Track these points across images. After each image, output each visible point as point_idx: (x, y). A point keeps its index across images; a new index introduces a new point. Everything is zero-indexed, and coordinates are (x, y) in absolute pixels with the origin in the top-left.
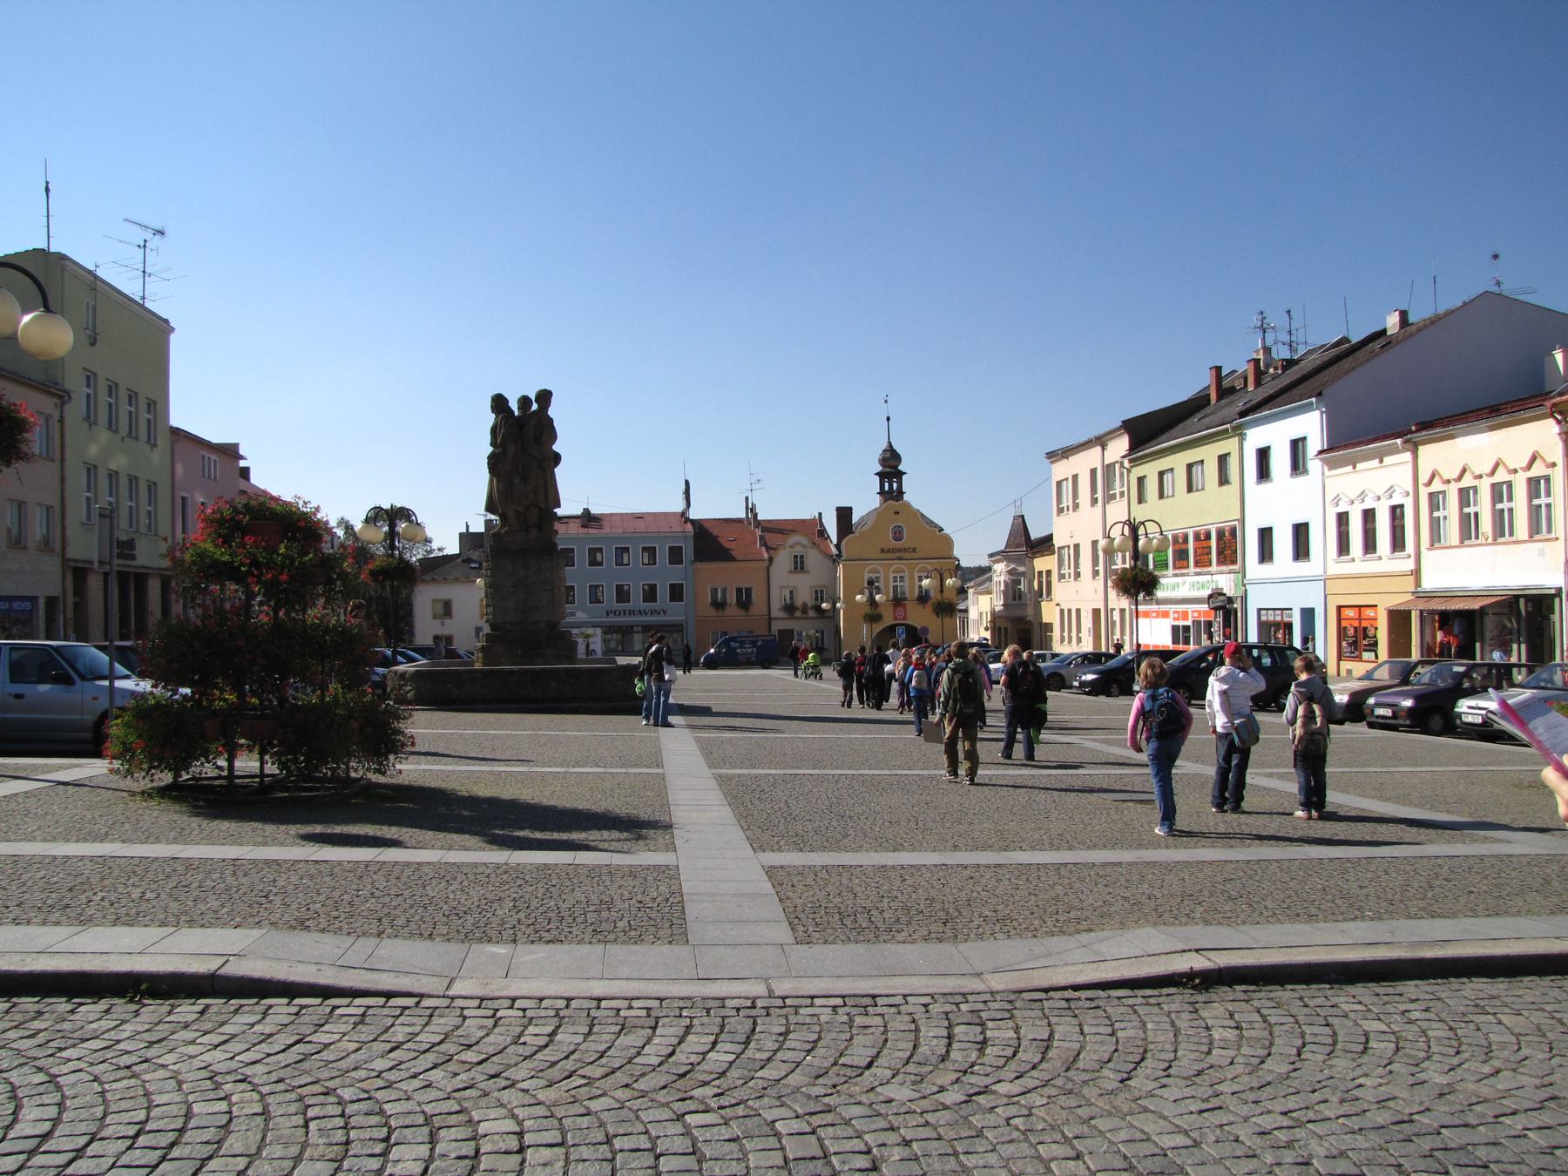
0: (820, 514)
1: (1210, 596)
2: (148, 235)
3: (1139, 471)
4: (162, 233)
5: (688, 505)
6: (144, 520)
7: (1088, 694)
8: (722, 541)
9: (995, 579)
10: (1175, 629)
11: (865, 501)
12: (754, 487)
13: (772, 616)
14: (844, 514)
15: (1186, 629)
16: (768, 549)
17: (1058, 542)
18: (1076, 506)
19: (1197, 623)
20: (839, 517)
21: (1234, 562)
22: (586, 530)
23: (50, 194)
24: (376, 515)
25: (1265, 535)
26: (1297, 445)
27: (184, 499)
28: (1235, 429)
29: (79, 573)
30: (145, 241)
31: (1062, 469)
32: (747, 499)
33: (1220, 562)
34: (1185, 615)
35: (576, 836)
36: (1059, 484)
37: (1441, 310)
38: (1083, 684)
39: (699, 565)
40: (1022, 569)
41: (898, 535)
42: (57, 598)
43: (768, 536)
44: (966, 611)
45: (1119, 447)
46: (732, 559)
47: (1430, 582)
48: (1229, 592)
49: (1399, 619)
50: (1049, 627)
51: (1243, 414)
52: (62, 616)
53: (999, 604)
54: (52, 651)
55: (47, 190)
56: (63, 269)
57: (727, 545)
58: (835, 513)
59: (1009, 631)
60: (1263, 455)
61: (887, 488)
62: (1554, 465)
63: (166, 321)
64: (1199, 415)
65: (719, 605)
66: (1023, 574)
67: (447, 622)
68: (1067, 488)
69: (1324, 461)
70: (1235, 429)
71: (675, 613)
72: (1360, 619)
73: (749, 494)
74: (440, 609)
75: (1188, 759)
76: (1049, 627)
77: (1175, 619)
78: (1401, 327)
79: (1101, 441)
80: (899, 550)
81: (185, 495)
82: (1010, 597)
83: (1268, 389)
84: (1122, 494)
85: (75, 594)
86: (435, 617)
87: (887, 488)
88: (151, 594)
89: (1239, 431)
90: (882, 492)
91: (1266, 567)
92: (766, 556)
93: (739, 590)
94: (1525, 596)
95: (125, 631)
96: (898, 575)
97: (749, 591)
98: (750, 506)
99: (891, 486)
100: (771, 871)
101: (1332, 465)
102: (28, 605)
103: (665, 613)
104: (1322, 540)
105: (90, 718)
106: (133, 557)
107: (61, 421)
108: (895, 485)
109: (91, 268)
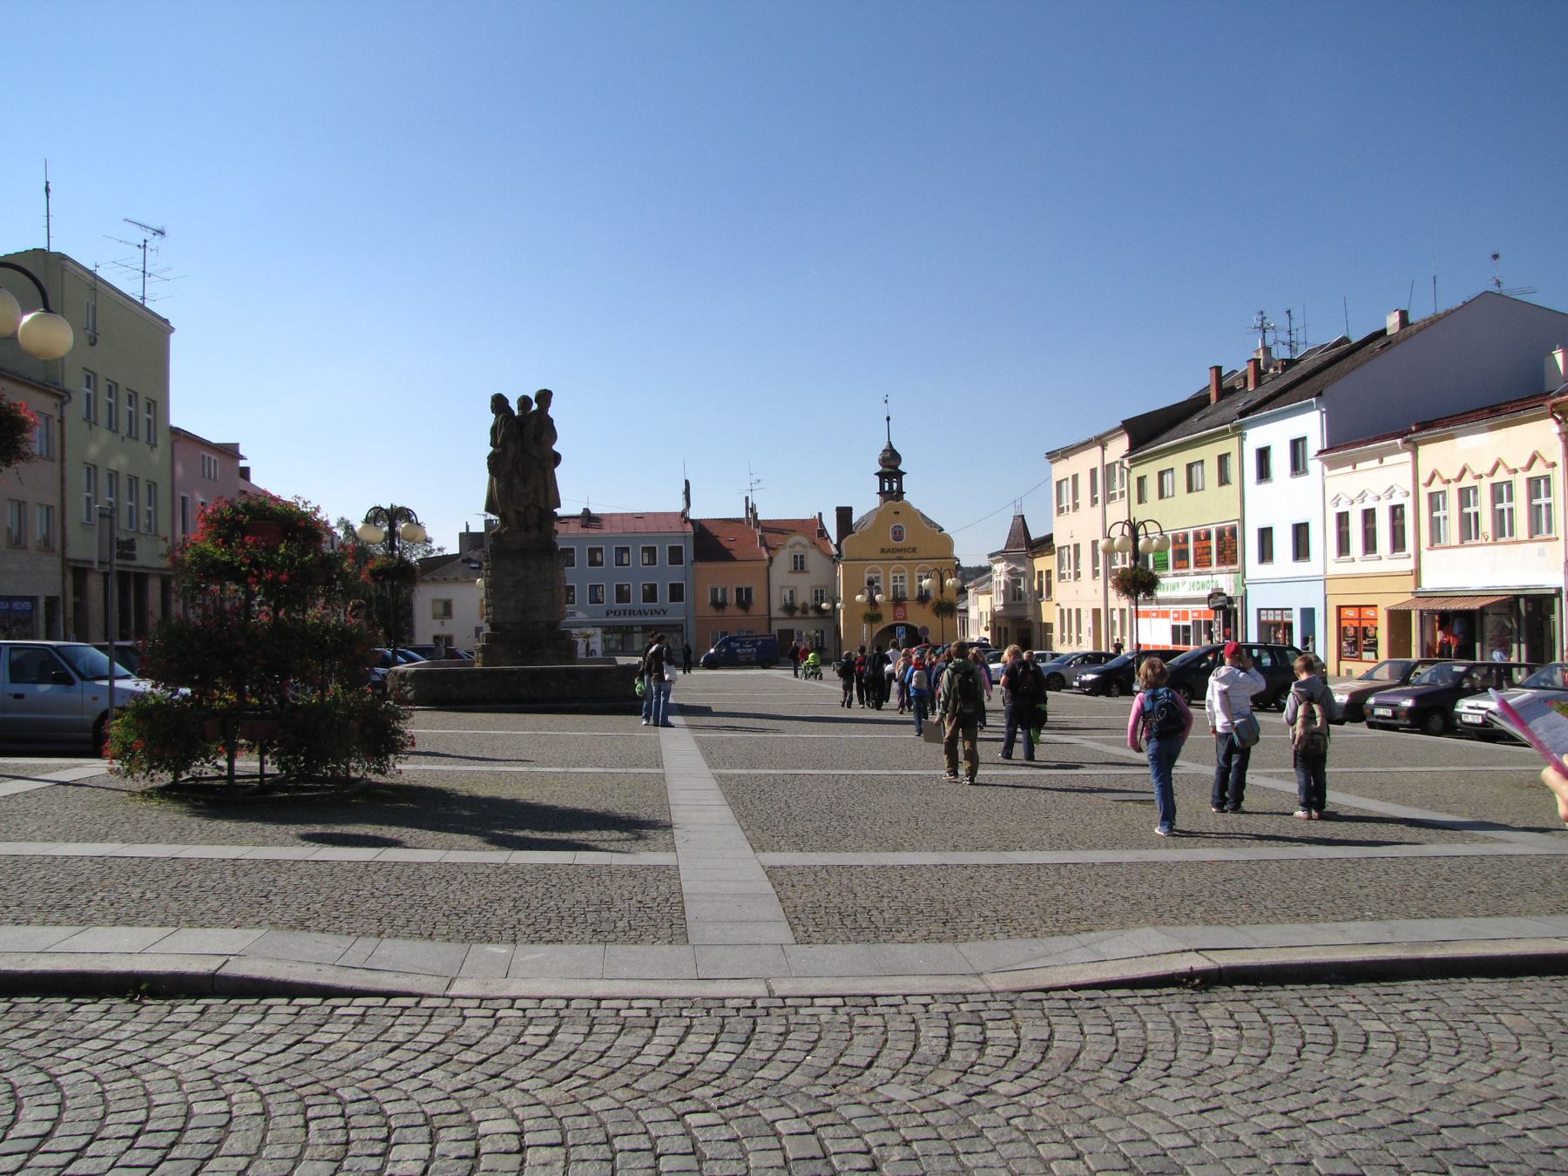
0: (820, 514)
1: (1210, 596)
2: (148, 235)
3: (1139, 471)
4: (162, 233)
5: (688, 505)
6: (144, 520)
7: (1088, 694)
8: (722, 541)
9: (995, 579)
10: (1175, 629)
11: (865, 501)
12: (754, 487)
13: (772, 616)
14: (844, 514)
15: (1186, 629)
16: (768, 549)
17: (1058, 542)
18: (1076, 506)
19: (1197, 623)
20: (839, 517)
21: (1234, 562)
22: (586, 530)
23: (50, 194)
24: (376, 515)
25: (1265, 535)
26: (1297, 445)
27: (184, 499)
28: (1235, 429)
29: (79, 573)
30: (145, 241)
31: (1062, 469)
32: (747, 499)
33: (1220, 562)
34: (1185, 615)
35: (576, 836)
36: (1059, 484)
37: (1441, 310)
38: (1083, 684)
39: (699, 565)
40: (1022, 569)
41: (898, 535)
42: (57, 598)
43: (768, 536)
44: (966, 611)
45: (1119, 447)
46: (732, 559)
47: (1430, 582)
48: (1229, 592)
49: (1399, 619)
50: (1049, 627)
51: (1243, 414)
52: (62, 616)
53: (999, 604)
54: (52, 651)
55: (47, 190)
56: (63, 269)
57: (727, 545)
58: (835, 513)
59: (1009, 631)
60: (1263, 455)
61: (887, 488)
62: (1554, 465)
63: (166, 321)
64: (1199, 415)
65: (719, 605)
66: (1023, 574)
67: (447, 622)
68: (1067, 488)
69: (1324, 461)
70: (1235, 429)
71: (675, 613)
72: (1360, 619)
73: (749, 494)
74: (440, 609)
75: (1188, 759)
76: (1049, 627)
77: (1175, 619)
78: (1401, 327)
79: (1101, 441)
80: (899, 550)
81: (185, 495)
82: (1010, 597)
83: (1268, 389)
84: (1122, 494)
85: (75, 594)
86: (435, 617)
87: (887, 488)
88: (151, 594)
89: (1239, 431)
90: (882, 492)
91: (1266, 567)
92: (766, 556)
93: (739, 590)
94: (1525, 596)
95: (125, 631)
96: (898, 575)
97: (749, 591)
98: (750, 506)
99: (891, 486)
100: (771, 871)
101: (1332, 465)
102: (28, 605)
103: (665, 613)
104: (1322, 540)
105: (90, 718)
106: (133, 557)
107: (61, 421)
108: (895, 485)
109: (91, 268)
